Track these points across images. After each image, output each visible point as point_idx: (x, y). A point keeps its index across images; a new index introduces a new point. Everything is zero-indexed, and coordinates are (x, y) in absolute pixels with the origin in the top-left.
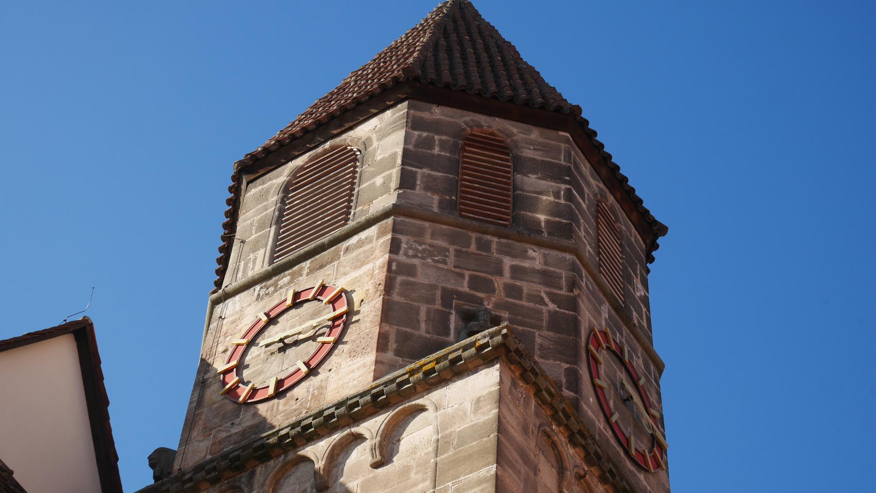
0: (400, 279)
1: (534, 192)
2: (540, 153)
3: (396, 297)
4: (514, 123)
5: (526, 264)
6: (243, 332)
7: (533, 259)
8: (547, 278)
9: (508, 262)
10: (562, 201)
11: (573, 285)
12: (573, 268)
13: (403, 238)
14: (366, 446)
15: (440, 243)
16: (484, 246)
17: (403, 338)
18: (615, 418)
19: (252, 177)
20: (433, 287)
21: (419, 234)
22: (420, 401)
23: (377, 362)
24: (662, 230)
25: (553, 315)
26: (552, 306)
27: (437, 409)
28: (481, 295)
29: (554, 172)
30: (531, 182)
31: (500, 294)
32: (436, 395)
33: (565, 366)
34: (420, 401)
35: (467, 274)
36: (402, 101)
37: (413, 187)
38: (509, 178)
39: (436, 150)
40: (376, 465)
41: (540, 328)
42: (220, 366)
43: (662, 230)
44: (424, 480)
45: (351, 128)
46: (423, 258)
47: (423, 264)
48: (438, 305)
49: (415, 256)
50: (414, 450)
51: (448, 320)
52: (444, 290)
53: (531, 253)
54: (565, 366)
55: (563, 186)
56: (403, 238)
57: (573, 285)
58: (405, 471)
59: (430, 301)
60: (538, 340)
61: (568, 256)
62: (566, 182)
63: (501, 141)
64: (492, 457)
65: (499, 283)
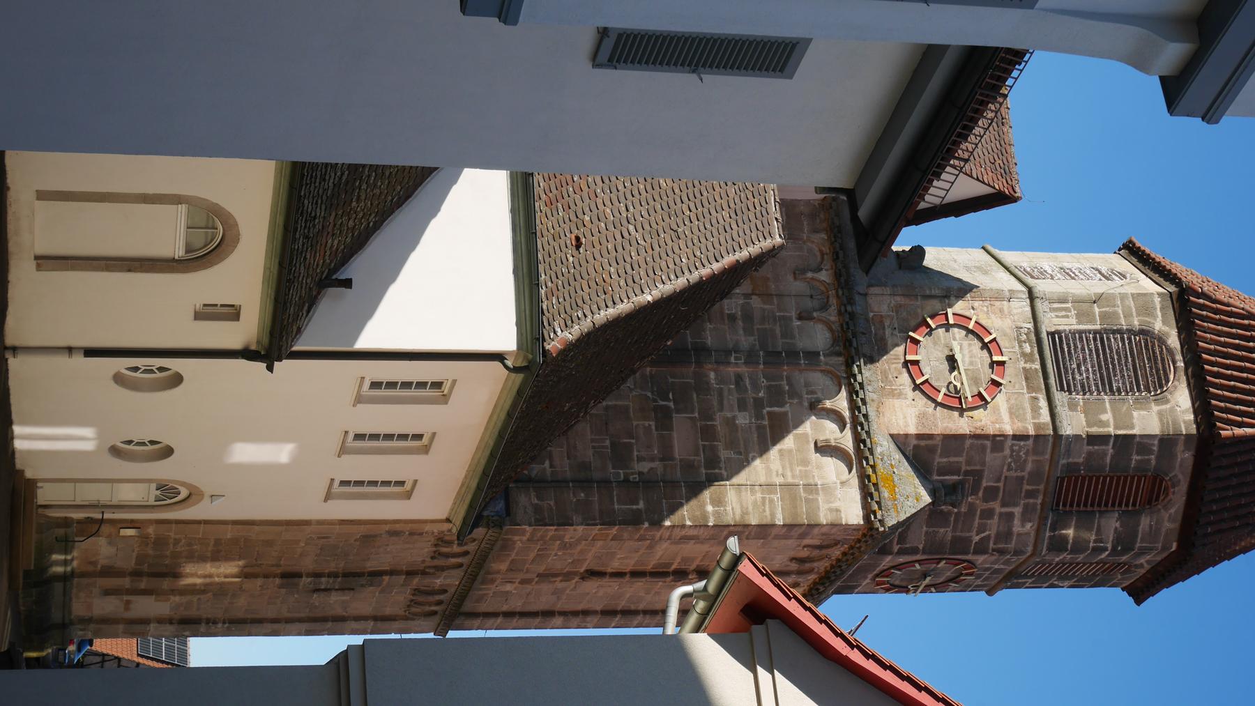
0: (988, 443)
1: (1099, 526)
2: (1147, 529)
3: (968, 442)
4: (1181, 511)
5: (1016, 522)
6: (983, 322)
7: (1023, 526)
8: (1006, 535)
9: (1017, 511)
10: (1091, 545)
11: (1002, 552)
12: (1017, 553)
13: (1030, 442)
14: (838, 434)
15: (1029, 467)
16: (1030, 494)
17: (931, 450)
18: (917, 566)
19: (1174, 297)
20: (983, 464)
21: (1035, 451)
22: (854, 470)
23: (906, 435)
24: (1139, 601)
25: (969, 540)
26: (977, 538)
27: (843, 483)
28: (980, 494)
29: (1125, 542)
30: (1112, 524)
31: (981, 506)
32: (855, 482)
33: (921, 547)
34: (854, 470)
35: (1001, 485)
36: (1198, 428)
37: (1088, 444)
38: (1113, 505)
39: (1135, 457)
40: (816, 443)
41: (954, 530)
42: (960, 307)
43: (1139, 601)
44: (793, 477)
45: (1189, 385)
46: (1011, 456)
47: (1005, 457)
48: (964, 468)
49: (1012, 451)
50: (819, 467)
51: (953, 474)
52: (982, 471)
53: (1029, 525)
54: (921, 547)
55: (1109, 546)
56: (1030, 442)
57: (1002, 552)
58: (805, 462)
59: (968, 463)
60: (942, 530)
61: (1030, 549)
62: (1114, 549)
63: (1157, 499)
64: (788, 521)
65: (996, 506)
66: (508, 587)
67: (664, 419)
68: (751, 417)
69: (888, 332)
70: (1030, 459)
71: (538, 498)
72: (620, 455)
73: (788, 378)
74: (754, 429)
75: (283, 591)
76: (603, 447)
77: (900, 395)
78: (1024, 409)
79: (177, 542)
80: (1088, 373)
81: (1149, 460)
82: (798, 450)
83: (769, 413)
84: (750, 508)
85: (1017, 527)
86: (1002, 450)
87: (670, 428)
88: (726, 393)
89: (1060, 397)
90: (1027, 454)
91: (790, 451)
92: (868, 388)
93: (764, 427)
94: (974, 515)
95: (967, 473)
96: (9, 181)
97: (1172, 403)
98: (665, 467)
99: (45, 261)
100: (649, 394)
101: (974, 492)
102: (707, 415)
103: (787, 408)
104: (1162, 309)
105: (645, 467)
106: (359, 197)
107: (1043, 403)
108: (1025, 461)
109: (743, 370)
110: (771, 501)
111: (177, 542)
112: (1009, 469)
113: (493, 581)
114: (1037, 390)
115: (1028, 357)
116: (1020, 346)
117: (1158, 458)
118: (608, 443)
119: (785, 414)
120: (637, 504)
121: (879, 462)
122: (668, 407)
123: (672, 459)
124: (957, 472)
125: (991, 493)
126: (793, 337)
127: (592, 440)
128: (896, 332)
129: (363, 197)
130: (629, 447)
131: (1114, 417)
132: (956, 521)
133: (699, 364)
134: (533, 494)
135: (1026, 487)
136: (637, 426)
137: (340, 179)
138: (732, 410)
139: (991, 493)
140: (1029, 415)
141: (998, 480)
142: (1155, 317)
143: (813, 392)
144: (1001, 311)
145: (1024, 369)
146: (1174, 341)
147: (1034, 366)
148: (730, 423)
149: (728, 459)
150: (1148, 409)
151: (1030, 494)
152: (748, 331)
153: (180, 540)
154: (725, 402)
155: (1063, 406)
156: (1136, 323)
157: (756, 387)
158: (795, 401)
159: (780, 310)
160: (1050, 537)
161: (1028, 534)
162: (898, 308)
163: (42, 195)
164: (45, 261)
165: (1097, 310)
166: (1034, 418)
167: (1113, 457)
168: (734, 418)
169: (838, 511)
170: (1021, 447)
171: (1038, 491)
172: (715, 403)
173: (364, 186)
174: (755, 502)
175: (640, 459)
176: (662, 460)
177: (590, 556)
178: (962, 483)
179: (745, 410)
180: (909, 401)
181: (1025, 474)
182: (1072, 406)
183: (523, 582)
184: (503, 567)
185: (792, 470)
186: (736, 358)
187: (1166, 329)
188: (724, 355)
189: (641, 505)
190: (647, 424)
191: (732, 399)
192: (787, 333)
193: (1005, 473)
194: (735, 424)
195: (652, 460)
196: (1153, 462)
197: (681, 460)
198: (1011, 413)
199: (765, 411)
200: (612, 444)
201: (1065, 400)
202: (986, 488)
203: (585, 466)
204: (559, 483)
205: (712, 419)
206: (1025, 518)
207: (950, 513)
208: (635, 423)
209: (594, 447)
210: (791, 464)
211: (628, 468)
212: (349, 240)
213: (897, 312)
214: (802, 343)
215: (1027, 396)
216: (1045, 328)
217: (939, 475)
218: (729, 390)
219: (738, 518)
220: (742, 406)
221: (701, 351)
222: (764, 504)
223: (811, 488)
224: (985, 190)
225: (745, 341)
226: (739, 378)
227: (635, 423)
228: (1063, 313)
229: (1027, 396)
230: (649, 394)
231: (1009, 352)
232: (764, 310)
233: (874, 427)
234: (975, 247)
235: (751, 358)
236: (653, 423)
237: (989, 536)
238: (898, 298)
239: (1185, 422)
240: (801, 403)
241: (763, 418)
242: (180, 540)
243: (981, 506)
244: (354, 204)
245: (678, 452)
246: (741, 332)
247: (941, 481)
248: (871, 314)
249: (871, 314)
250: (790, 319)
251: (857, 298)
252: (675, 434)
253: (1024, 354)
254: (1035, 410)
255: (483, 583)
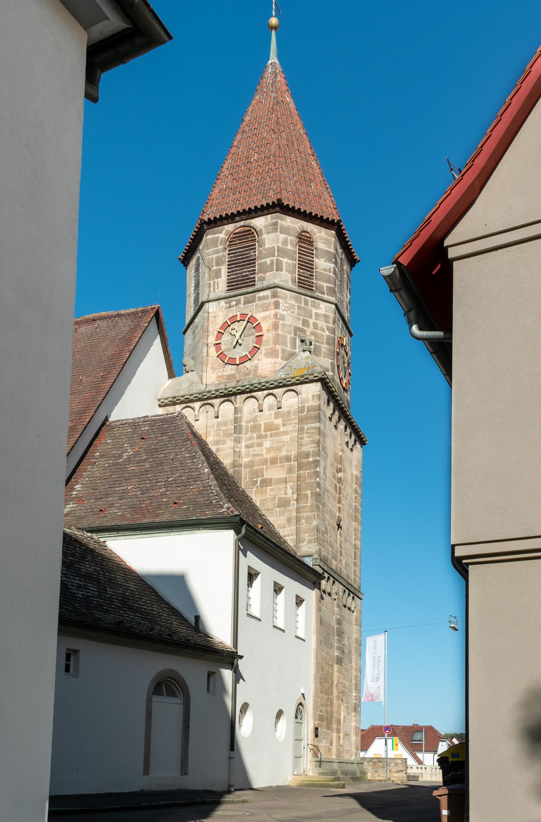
2: (324, 245)
5: (319, 311)
7: (322, 308)
9: (314, 311)
15: (293, 302)
16: (306, 303)
20: (291, 326)
25: (328, 337)
28: (305, 328)
35: (301, 318)
41: (322, 343)
44: (296, 419)
45: (252, 218)
46: (287, 311)
47: (288, 314)
48: (293, 336)
49: (285, 310)
58: (289, 413)
59: (290, 333)
60: (323, 349)
63: (310, 238)
65: (311, 321)
66: (343, 562)
67: (266, 482)
68: (266, 440)
69: (225, 373)
70: (289, 302)
71: (304, 542)
72: (284, 503)
73: (247, 422)
74: (272, 439)
75: (343, 664)
76: (280, 511)
77: (256, 367)
78: (264, 304)
79: (321, 711)
80: (245, 271)
81: (291, 240)
82: (283, 417)
83: (264, 431)
84: (311, 439)
85: (322, 311)
86: (284, 315)
87: (271, 479)
88: (254, 453)
89: (258, 285)
90: (286, 303)
91: (283, 421)
92: (253, 382)
93: (271, 434)
94: (316, 332)
95: (295, 334)
96: (138, 790)
97: (262, 227)
98: (290, 481)
99: (184, 771)
100: (254, 490)
101: (304, 331)
102: (265, 462)
103: (262, 423)
104: (214, 234)
105: (290, 491)
106: (150, 610)
107: (262, 294)
108: (290, 304)
109: (243, 444)
110: (308, 429)
111: (321, 711)
112: (294, 313)
113: (341, 569)
114: (255, 297)
115: (238, 302)
116: (233, 306)
117: (290, 235)
118: (278, 509)
119: (265, 423)
120: (308, 494)
121: (291, 376)
122: (261, 481)
123: (286, 478)
124: (295, 339)
125: (305, 323)
126: (227, 421)
127: (276, 516)
128: (225, 369)
129: (151, 608)
130: (280, 499)
131: (269, 257)
132: (318, 342)
133: (240, 465)
134: (302, 544)
135: (303, 305)
136: (270, 495)
137: (140, 617)
138: (262, 450)
139: (305, 323)
140: (267, 301)
141: (299, 319)
142: (218, 237)
143: (254, 410)
144: (215, 317)
145: (244, 304)
146: (230, 227)
147: (242, 300)
148: (269, 450)
149: (287, 451)
150: (264, 240)
151: (306, 303)
152: (224, 442)
153: (320, 710)
154: (259, 453)
155: (263, 284)
156: (221, 247)
157: (251, 438)
158: (258, 419)
159: (214, 427)
160: (328, 295)
161: (326, 306)
162: (213, 369)
163: (146, 771)
164: (184, 771)
165: (215, 268)
166: (268, 299)
167: (289, 259)
168: (266, 449)
169: (313, 396)
170: (283, 306)
171: (305, 299)
172: (259, 458)
173: (145, 607)
174: (308, 437)
175: (286, 493)
176: (286, 483)
177: (331, 522)
178: (299, 337)
179: (262, 443)
180: (259, 362)
181: (296, 305)
182: (262, 279)
183: (341, 555)
184: (334, 563)
185: (293, 420)
186: (237, 448)
187: (224, 232)
188: (237, 454)
189: (309, 492)
190: (269, 491)
191: (257, 450)
192: (225, 424)
193: (295, 315)
194: (269, 448)
195: (286, 487)
196: (292, 238)
197: (287, 474)
198: (266, 310)
199: (263, 434)
200: (278, 507)
201: (259, 282)
202: (303, 325)
203: (289, 520)
204: (298, 532)
205: (267, 459)
206: (317, 307)
207: (315, 345)
208: (268, 496)
209: (280, 516)
210: (290, 420)
211: (290, 500)
212: (174, 617)
213: (215, 369)
214: (231, 416)
215: (257, 302)
216: (224, 295)
217: (296, 348)
218: (253, 451)
219: (316, 445)
220: (260, 445)
221: (235, 465)
222: (309, 433)
223: (301, 410)
224: (154, 322)
225: (230, 443)
226: (247, 447)
227: (268, 496)
228: (216, 285)
229: (257, 302)
230: (254, 490)
231: (235, 312)
232: (214, 435)
233: (272, 379)
234: (184, 337)
235: (237, 441)
236: (269, 488)
237: (327, 326)
238: (208, 369)
239: (272, 220)
240: (260, 416)
241: (267, 434)
242: (320, 710)
243: (311, 329)
244: (155, 613)
245: (283, 476)
246: (224, 446)
247: (299, 347)
248: (216, 382)
249: (216, 382)
250: (218, 422)
251: (208, 389)
252: (274, 477)
253: (236, 305)
254: (264, 298)
255: (341, 574)
